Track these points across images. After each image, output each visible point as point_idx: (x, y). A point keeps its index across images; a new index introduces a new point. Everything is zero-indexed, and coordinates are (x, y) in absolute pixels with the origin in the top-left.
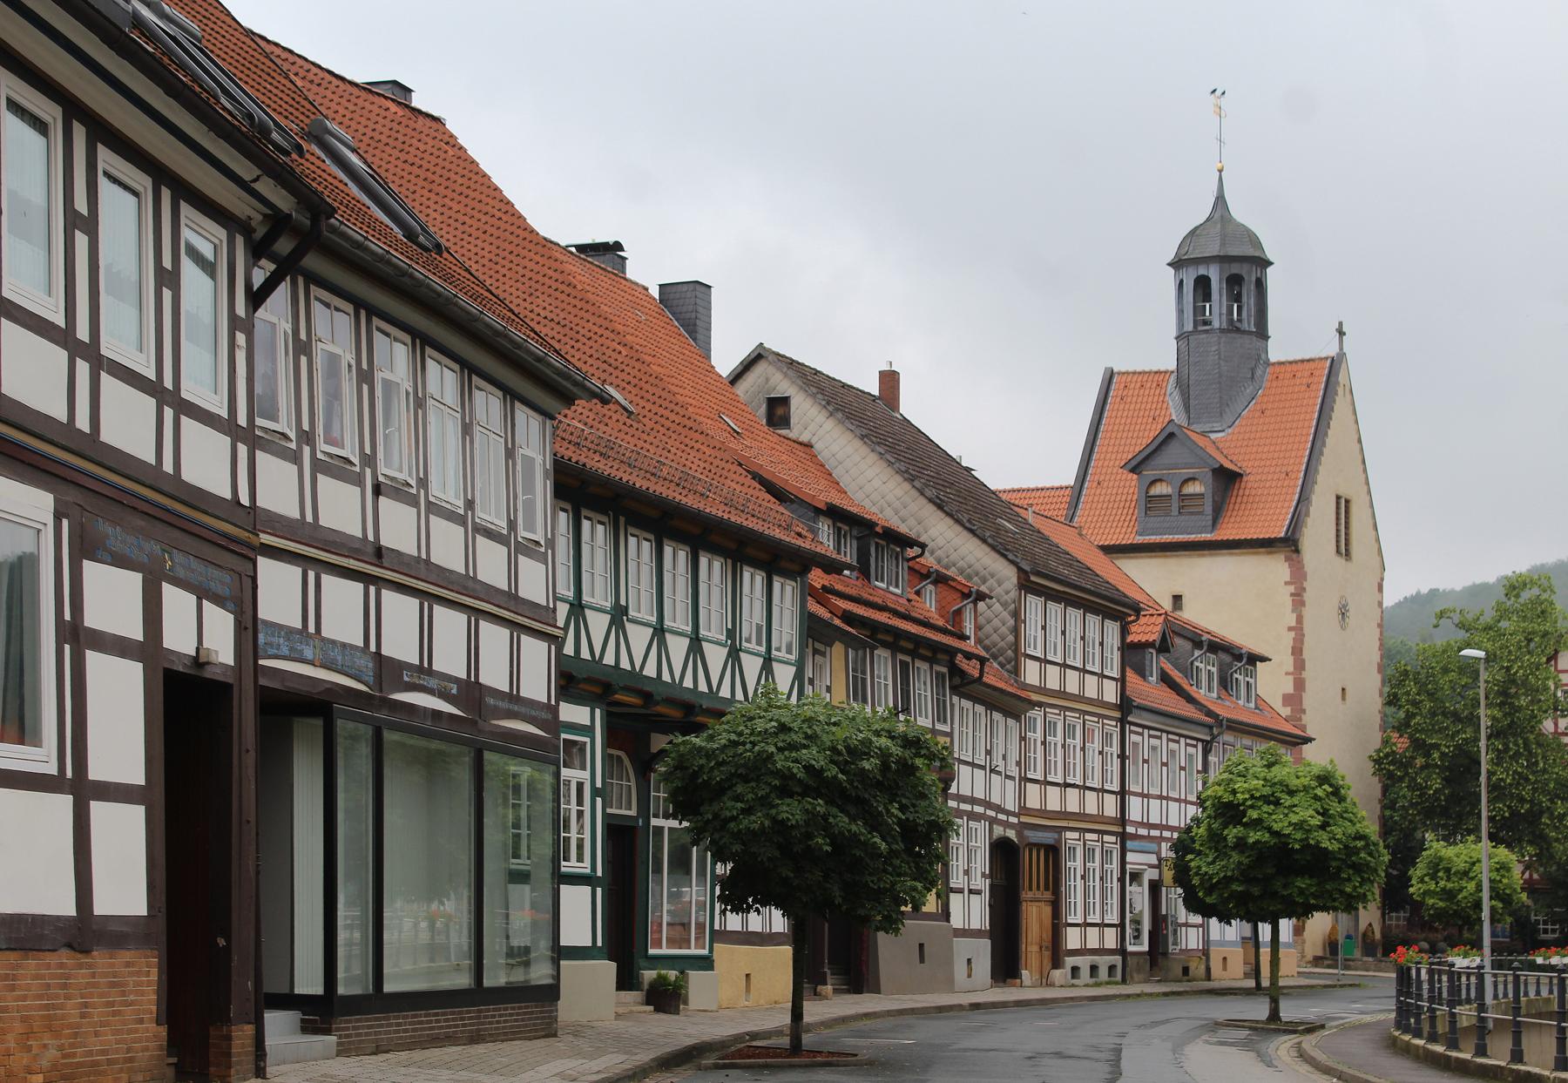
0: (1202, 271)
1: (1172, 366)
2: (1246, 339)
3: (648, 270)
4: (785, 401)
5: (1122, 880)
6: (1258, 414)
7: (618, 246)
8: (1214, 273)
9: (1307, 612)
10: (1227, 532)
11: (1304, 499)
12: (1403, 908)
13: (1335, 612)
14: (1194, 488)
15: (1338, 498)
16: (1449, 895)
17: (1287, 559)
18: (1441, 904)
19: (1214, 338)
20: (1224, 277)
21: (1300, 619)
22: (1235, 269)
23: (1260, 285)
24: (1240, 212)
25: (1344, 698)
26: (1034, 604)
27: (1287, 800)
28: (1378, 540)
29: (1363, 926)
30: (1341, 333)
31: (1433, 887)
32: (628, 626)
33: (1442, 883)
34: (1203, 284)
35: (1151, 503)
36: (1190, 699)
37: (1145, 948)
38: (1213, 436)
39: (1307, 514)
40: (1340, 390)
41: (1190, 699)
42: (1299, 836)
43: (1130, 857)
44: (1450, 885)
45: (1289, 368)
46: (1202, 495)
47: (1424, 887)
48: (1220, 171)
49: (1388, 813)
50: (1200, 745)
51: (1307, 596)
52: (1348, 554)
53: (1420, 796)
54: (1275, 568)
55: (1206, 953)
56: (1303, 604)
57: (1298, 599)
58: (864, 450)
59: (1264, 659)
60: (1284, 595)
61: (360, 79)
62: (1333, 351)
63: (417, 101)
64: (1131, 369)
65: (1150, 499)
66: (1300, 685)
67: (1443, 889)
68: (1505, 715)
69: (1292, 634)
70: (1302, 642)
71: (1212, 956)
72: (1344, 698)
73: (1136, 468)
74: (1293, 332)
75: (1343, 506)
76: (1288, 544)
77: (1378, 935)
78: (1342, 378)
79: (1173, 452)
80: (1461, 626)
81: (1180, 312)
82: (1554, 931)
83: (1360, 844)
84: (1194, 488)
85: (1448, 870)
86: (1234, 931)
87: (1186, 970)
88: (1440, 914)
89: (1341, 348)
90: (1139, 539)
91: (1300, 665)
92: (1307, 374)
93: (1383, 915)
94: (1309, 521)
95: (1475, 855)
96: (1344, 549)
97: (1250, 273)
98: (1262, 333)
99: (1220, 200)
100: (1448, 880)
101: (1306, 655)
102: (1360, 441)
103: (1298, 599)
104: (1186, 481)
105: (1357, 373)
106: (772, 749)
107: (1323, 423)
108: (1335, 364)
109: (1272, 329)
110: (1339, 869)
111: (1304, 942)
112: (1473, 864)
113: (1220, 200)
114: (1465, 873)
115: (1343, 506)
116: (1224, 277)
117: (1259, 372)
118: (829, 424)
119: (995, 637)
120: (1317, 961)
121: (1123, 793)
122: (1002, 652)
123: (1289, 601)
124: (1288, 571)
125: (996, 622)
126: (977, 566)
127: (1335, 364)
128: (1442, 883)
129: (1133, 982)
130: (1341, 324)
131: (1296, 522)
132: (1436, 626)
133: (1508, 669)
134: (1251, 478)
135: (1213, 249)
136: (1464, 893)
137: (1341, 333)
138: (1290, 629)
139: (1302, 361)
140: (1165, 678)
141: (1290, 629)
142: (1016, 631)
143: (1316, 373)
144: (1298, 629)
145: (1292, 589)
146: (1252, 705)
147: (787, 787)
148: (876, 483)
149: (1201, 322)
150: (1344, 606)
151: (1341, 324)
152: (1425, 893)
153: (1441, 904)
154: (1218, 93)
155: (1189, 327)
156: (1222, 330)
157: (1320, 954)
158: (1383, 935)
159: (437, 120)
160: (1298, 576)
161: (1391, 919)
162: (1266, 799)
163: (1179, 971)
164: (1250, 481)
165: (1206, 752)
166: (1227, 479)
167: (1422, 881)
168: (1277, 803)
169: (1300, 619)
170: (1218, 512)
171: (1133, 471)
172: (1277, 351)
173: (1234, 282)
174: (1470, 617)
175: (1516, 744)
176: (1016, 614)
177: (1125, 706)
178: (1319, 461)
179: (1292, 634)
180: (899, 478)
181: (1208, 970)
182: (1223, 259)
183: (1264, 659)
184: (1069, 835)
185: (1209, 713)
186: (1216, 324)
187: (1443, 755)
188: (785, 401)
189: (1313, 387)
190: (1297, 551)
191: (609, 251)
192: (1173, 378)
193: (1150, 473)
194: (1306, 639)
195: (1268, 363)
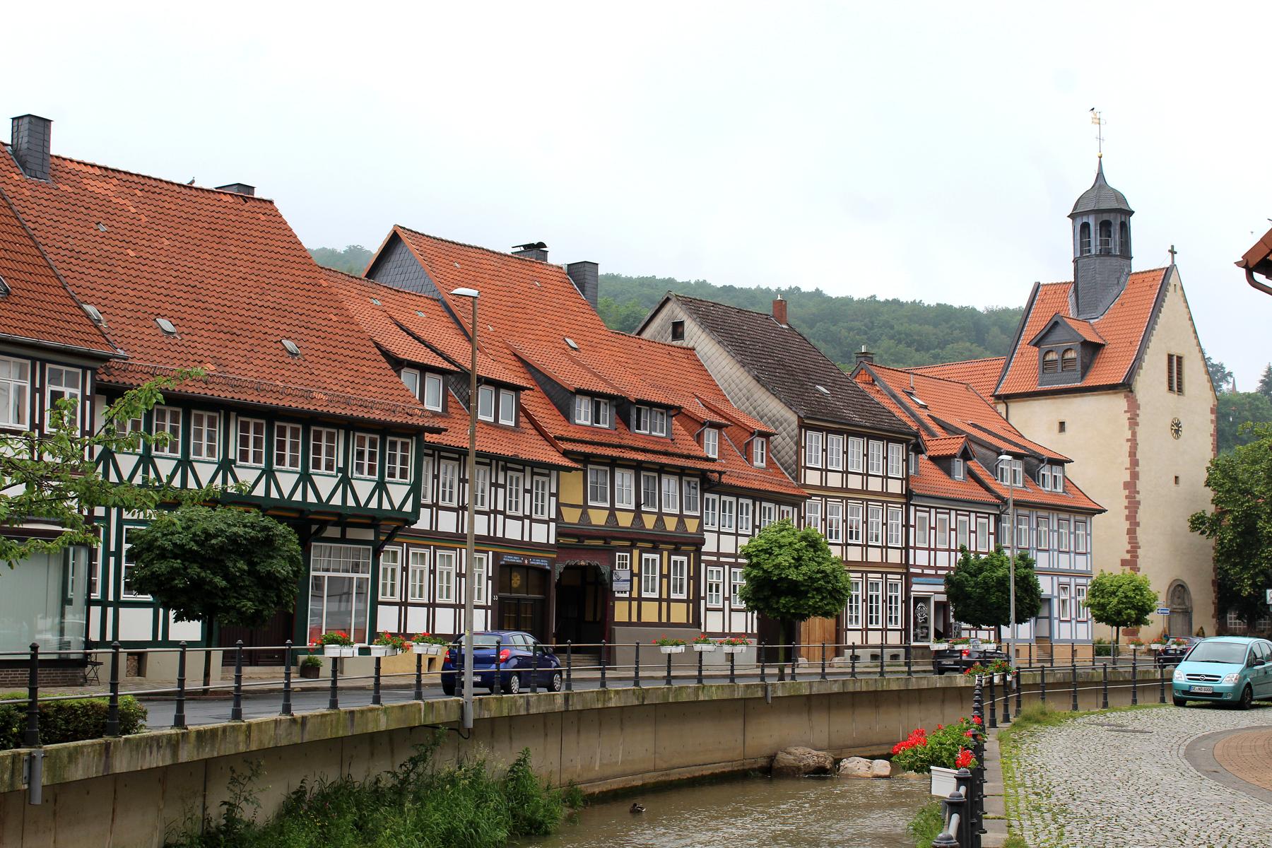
0: (1085, 220)
2: (1113, 260)
3: (558, 257)
4: (681, 323)
5: (906, 602)
7: (541, 245)
8: (1091, 221)
10: (1091, 381)
15: (1170, 357)
17: (1126, 397)
20: (1103, 223)
21: (1134, 434)
22: (1106, 217)
23: (1125, 228)
24: (1112, 181)
26: (814, 440)
27: (776, 551)
30: (1173, 252)
32: (236, 470)
34: (1085, 227)
35: (1046, 365)
36: (988, 489)
41: (988, 489)
42: (776, 572)
43: (914, 587)
50: (992, 518)
52: (1180, 390)
54: (1118, 403)
56: (1137, 424)
57: (1133, 422)
58: (721, 350)
59: (1071, 461)
60: (1124, 419)
61: (211, 185)
62: (1168, 264)
63: (257, 194)
66: (1135, 476)
73: (1037, 343)
76: (1125, 387)
79: (1058, 334)
83: (819, 576)
90: (1039, 388)
91: (1134, 462)
98: (1126, 254)
99: (1100, 175)
102: (1191, 319)
103: (1133, 422)
104: (1066, 351)
106: (159, 535)
108: (1168, 271)
110: (807, 592)
113: (1100, 175)
116: (1103, 223)
117: (1122, 280)
118: (704, 336)
119: (787, 458)
121: (906, 548)
122: (790, 466)
125: (787, 448)
126: (778, 416)
137: (1173, 252)
140: (971, 474)
142: (798, 453)
144: (1133, 441)
145: (1128, 415)
146: (1060, 489)
147: (163, 555)
148: (727, 369)
150: (1177, 425)
159: (271, 202)
160: (1133, 408)
162: (765, 551)
165: (998, 520)
166: (1093, 349)
168: (770, 554)
171: (1035, 345)
172: (1137, 265)
173: (1105, 226)
176: (798, 443)
177: (908, 497)
180: (738, 366)
182: (1097, 212)
184: (852, 575)
185: (998, 497)
186: (1093, 252)
188: (681, 323)
190: (1131, 391)
191: (537, 249)
193: (1045, 347)
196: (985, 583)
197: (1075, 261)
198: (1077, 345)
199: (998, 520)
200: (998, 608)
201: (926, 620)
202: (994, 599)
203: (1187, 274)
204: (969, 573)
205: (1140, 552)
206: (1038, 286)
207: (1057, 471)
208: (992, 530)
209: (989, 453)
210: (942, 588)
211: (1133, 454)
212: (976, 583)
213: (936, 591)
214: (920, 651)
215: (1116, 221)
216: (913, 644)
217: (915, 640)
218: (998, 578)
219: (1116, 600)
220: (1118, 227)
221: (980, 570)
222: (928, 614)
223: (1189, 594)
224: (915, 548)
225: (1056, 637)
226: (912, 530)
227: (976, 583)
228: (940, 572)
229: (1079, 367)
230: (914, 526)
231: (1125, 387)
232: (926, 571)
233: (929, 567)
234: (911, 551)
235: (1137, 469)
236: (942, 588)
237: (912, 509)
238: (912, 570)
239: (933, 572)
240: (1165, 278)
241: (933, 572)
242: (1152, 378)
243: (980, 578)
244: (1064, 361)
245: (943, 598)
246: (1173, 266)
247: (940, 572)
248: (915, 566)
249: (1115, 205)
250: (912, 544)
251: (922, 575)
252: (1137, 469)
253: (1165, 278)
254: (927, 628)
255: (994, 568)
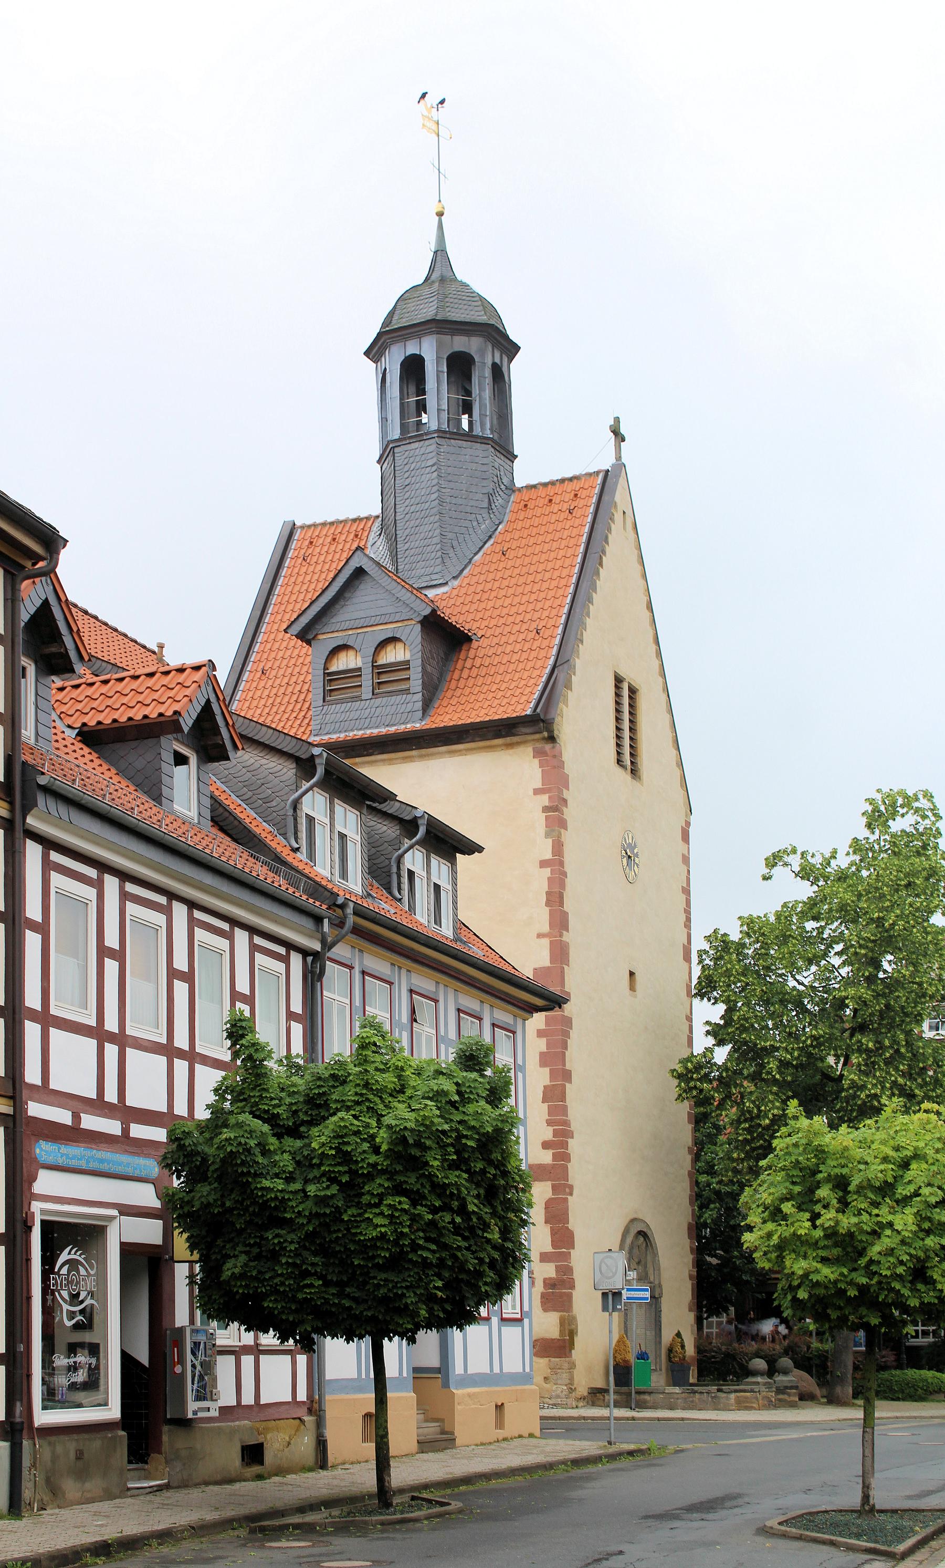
0: (412, 348)
1: (377, 511)
6: (496, 557)
8: (429, 350)
9: (570, 838)
10: (448, 715)
11: (562, 663)
12: (726, 1310)
13: (616, 853)
14: (393, 655)
16: (847, 1247)
17: (538, 753)
18: (827, 1273)
19: (430, 446)
21: (558, 848)
22: (460, 343)
25: (632, 988)
28: (680, 764)
29: (667, 1336)
31: (803, 1227)
33: (828, 1217)
34: (413, 369)
35: (335, 684)
37: (113, 1411)
38: (431, 593)
39: (568, 686)
40: (618, 517)
43: (46, 1183)
44: (847, 1222)
45: (542, 492)
46: (404, 666)
47: (780, 1231)
48: (440, 214)
49: (703, 1178)
51: (570, 813)
52: (634, 772)
53: (749, 1130)
55: (315, 1407)
56: (563, 824)
60: (533, 811)
62: (607, 462)
64: (319, 520)
65: (330, 677)
67: (831, 1234)
68: (877, 996)
69: (547, 872)
70: (562, 885)
71: (330, 1414)
72: (632, 988)
73: (306, 635)
74: (548, 441)
75: (626, 696)
76: (534, 728)
77: (690, 1350)
78: (619, 496)
79: (365, 603)
80: (806, 873)
81: (384, 420)
82: (925, 1333)
84: (393, 655)
85: (841, 1184)
86: (343, 1357)
87: (253, 1454)
88: (824, 1305)
89: (619, 458)
92: (568, 497)
93: (699, 1321)
94: (572, 696)
95: (909, 1143)
96: (629, 758)
97: (482, 352)
98: (504, 448)
99: (440, 255)
100: (844, 1205)
101: (569, 905)
102: (686, 891)
105: (644, 492)
107: (591, 557)
108: (608, 480)
109: (519, 445)
111: (573, 1366)
112: (905, 1165)
113: (440, 255)
114: (886, 1189)
115: (626, 696)
116: (446, 359)
117: (499, 501)
120: (596, 1395)
123: (540, 819)
124: (538, 772)
127: (608, 480)
128: (828, 1217)
129: (55, 1494)
130: (617, 420)
131: (551, 692)
132: (766, 878)
133: (879, 921)
134: (484, 642)
135: (427, 311)
136: (887, 1240)
138: (543, 864)
139: (563, 481)
141: (543, 864)
143: (582, 494)
144: (556, 865)
145: (544, 800)
149: (412, 432)
151: (617, 420)
152: (781, 1247)
153: (827, 1273)
154: (432, 99)
155: (396, 434)
156: (441, 434)
157: (600, 1384)
158: (699, 1350)
160: (555, 784)
161: (710, 1326)
163: (233, 1458)
164: (480, 649)
165: (313, 979)
166: (446, 638)
167: (776, 1214)
169: (558, 848)
170: (431, 693)
172: (525, 473)
173: (460, 367)
174: (817, 861)
175: (895, 1042)
178: (585, 607)
179: (547, 872)
181: (321, 1444)
182: (441, 326)
183: (471, 848)
187: (784, 1064)
189: (578, 513)
190: (552, 739)
192: (378, 523)
193: (328, 640)
194: (568, 881)
195: (511, 489)
196: (345, 1157)
197: (388, 452)
198: (413, 633)
199: (313, 979)
200: (396, 1263)
201: (88, 1320)
202: (379, 1225)
203: (648, 495)
204: (271, 1119)
205: (574, 1145)
206: (290, 532)
207: (439, 869)
208: (297, 1007)
209: (272, 764)
210: (147, 1196)
211: (555, 899)
212: (305, 1163)
213: (124, 1201)
214: (69, 1446)
215: (485, 356)
216: (43, 1417)
217: (51, 1399)
218: (400, 1139)
219: (905, 1220)
220: (488, 373)
221: (317, 1106)
222: (100, 1293)
223: (655, 1255)
224: (46, 1020)
225: (459, 1369)
226: (32, 941)
227: (305, 1163)
228: (138, 1131)
229: (416, 683)
230: (43, 929)
231: (534, 728)
232: (90, 1122)
233: (99, 1105)
234: (32, 1031)
235: (566, 937)
236: (147, 1196)
237: (33, 852)
238: (35, 1109)
239: (113, 1127)
240: (599, 499)
241: (113, 1127)
242: (584, 720)
243: (320, 1138)
244: (379, 670)
245: (149, 1232)
246: (620, 466)
247: (138, 1131)
248: (45, 1092)
249: (483, 319)
250: (32, 999)
251: (72, 1134)
252: (566, 937)
253: (599, 499)
254: (94, 1350)
255: (370, 1098)
